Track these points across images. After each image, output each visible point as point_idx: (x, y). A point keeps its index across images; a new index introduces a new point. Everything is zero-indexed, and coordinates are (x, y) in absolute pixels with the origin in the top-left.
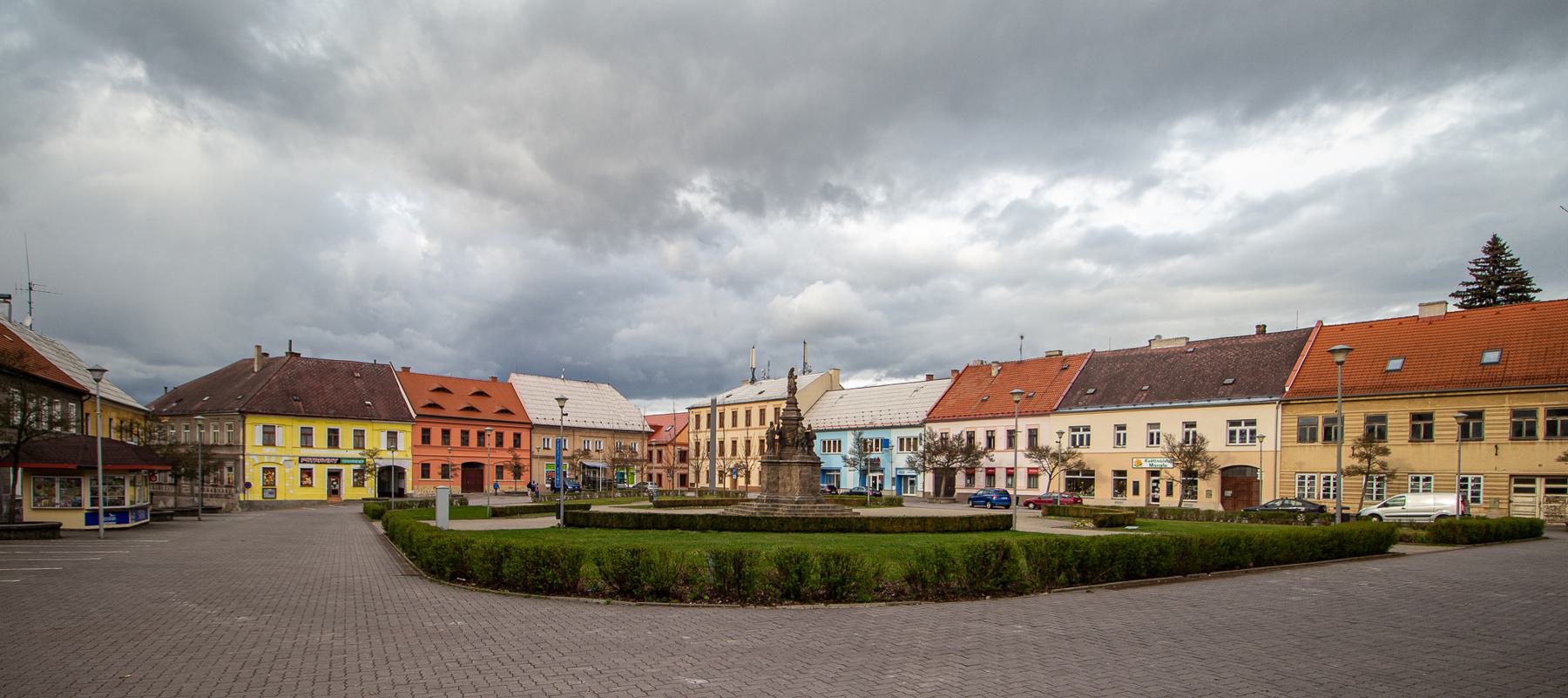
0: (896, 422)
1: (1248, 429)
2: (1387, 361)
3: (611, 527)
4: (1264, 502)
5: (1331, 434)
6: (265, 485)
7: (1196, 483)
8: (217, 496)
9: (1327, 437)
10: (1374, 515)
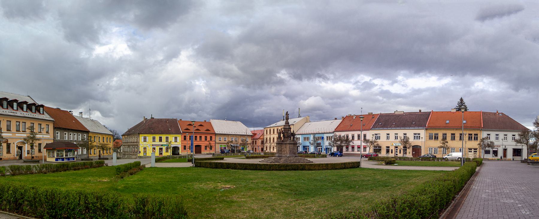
0: (325, 132)
3: (207, 167)
4: (423, 154)
5: (436, 138)
6: (144, 152)
9: (435, 139)
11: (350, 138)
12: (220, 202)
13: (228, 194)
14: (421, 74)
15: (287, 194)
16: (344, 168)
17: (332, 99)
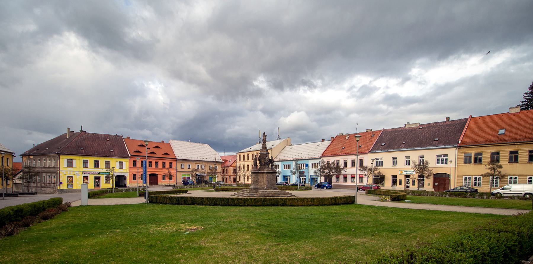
0: (310, 157)
1: (444, 158)
2: (498, 130)
3: (166, 204)
4: (452, 186)
5: (478, 160)
6: (69, 183)
7: (423, 180)
8: (50, 187)
9: (476, 161)
10: (499, 193)
11: (342, 164)
12: (185, 249)
13: (195, 238)
14: (451, 57)
15: (266, 236)
16: (335, 204)
17: (318, 114)
